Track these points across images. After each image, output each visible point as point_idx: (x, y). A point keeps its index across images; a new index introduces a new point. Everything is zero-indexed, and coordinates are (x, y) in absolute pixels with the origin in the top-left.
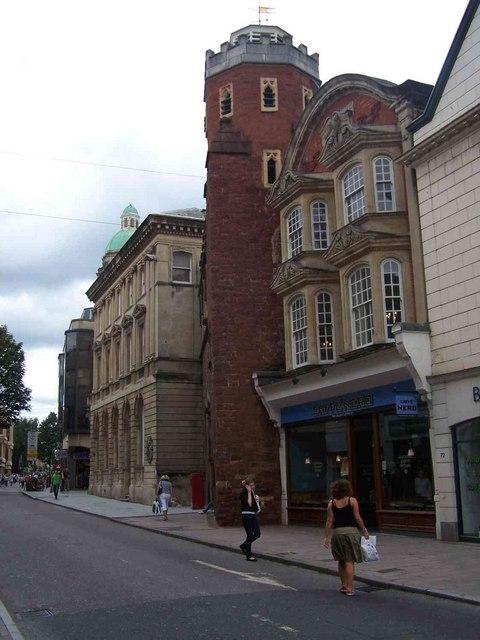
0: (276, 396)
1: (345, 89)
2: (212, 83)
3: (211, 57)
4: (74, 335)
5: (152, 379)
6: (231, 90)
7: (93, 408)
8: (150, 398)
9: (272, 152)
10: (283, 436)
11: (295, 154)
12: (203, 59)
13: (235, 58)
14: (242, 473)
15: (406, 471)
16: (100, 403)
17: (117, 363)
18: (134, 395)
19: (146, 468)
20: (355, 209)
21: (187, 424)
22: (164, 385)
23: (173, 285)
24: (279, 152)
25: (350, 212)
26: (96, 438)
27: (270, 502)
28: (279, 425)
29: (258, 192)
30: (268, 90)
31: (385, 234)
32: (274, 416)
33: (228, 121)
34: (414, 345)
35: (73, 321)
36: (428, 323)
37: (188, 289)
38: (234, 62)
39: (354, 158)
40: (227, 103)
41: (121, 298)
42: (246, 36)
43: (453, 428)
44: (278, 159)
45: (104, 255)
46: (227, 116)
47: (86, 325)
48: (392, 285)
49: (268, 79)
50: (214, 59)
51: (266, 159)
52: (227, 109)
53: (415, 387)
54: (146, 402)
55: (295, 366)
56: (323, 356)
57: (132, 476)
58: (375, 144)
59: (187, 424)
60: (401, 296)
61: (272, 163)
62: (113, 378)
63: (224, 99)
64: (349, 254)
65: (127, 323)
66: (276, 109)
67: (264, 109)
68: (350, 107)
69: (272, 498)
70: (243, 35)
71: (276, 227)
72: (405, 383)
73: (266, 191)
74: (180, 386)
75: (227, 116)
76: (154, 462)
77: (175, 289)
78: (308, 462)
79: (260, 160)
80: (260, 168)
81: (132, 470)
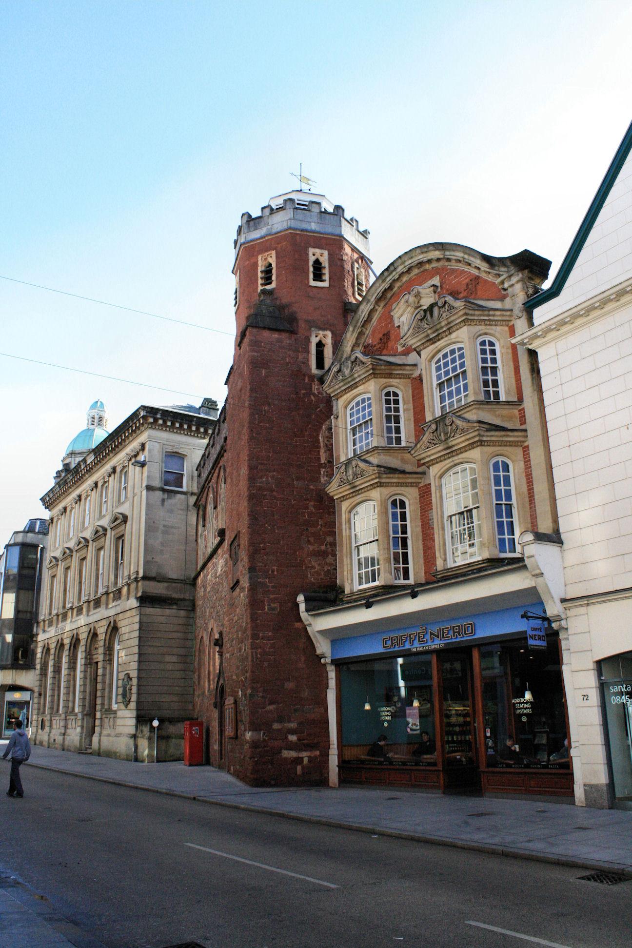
0: (321, 624)
1: (429, 261)
2: (247, 254)
3: (250, 221)
4: (16, 551)
5: (133, 603)
6: (273, 260)
7: (41, 637)
8: (130, 627)
9: (321, 332)
10: (332, 675)
11: (355, 335)
13: (279, 223)
14: (281, 720)
15: (386, 724)
16: (52, 632)
17: (80, 583)
18: (105, 622)
19: (119, 713)
20: (361, 441)
21: (174, 659)
22: (149, 610)
23: (163, 490)
24: (329, 334)
25: (354, 444)
26: (44, 673)
27: (316, 757)
28: (329, 660)
29: (300, 374)
30: (317, 263)
31: (496, 426)
32: (323, 647)
33: (270, 293)
34: (541, 555)
35: (16, 533)
36: (557, 531)
37: (182, 497)
38: (277, 227)
39: (454, 335)
40: (268, 272)
41: (90, 504)
43: (599, 663)
44: (328, 341)
45: (64, 455)
46: (268, 287)
47: (31, 538)
48: (503, 488)
49: (318, 251)
50: (252, 223)
51: (314, 341)
52: (268, 279)
53: (315, 651)
54: (123, 630)
55: (357, 587)
56: (502, 550)
57: (97, 722)
58: (480, 320)
59: (174, 659)
60: (514, 501)
61: (320, 345)
62: (72, 600)
63: (263, 269)
65: (100, 534)
66: (326, 284)
67: (313, 283)
68: (436, 281)
69: (318, 753)
72: (530, 602)
73: (312, 377)
74: (168, 611)
75: (268, 287)
76: (133, 705)
77: (166, 496)
78: (367, 707)
79: (308, 340)
80: (308, 351)
81: (98, 715)
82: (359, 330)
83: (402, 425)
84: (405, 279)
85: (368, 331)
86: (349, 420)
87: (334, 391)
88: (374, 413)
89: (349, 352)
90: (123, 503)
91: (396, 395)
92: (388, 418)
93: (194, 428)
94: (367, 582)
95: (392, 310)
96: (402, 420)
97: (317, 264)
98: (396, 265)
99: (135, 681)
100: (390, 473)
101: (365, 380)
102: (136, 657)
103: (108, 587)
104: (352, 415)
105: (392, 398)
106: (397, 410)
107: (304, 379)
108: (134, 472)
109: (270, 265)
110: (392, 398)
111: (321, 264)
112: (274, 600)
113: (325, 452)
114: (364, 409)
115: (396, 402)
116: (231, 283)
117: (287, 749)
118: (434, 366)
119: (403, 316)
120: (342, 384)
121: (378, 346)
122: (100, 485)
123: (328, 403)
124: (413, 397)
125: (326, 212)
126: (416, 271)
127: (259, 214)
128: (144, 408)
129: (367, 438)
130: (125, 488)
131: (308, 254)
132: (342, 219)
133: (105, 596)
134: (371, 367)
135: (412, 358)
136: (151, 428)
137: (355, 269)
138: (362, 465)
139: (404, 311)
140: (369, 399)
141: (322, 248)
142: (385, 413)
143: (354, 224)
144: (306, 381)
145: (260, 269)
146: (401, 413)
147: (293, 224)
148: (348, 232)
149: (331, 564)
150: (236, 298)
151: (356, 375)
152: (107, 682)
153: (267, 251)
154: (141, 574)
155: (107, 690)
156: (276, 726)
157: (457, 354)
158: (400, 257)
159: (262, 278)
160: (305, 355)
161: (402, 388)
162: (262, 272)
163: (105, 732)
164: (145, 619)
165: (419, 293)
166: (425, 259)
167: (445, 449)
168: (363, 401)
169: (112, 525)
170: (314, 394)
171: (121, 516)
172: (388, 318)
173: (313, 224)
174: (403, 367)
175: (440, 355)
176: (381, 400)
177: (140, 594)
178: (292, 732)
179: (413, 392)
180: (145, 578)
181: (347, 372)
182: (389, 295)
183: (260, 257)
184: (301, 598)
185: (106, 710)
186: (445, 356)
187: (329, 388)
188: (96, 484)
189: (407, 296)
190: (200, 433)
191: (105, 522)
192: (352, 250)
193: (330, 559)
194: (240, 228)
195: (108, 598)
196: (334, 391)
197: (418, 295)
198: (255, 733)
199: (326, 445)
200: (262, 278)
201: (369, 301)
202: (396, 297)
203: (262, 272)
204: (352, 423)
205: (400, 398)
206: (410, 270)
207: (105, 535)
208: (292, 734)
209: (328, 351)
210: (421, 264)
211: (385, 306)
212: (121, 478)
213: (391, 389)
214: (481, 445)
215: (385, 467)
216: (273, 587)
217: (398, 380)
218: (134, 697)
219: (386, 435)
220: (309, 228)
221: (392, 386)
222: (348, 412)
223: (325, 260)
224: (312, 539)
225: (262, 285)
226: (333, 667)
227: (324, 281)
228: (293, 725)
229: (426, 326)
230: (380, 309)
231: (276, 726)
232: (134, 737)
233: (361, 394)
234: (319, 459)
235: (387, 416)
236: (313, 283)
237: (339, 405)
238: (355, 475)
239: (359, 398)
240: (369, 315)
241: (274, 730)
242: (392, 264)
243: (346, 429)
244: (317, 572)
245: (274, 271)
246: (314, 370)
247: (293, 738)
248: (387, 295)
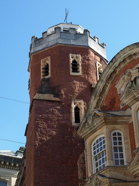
2: (35, 58)
3: (36, 41)
6: (49, 62)
11: (96, 101)
12: (30, 42)
13: (52, 41)
25: (97, 166)
33: (48, 80)
40: (46, 68)
42: (60, 28)
44: (82, 106)
46: (46, 77)
49: (75, 56)
50: (37, 42)
52: (46, 73)
61: (77, 109)
63: (44, 67)
64: (90, 129)
66: (49, 76)
67: (72, 74)
70: (58, 27)
71: (81, 153)
73: (73, 128)
75: (46, 77)
80: (70, 113)
82: (98, 98)
83: (124, 152)
84: (122, 66)
85: (103, 99)
86: (93, 151)
87: (83, 135)
88: (106, 146)
91: (119, 134)
92: (115, 149)
93: (12, 164)
95: (115, 85)
96: (124, 150)
97: (75, 63)
98: (116, 58)
100: (117, 182)
101: (100, 127)
104: (94, 148)
105: (117, 136)
106: (120, 143)
107: (68, 129)
109: (48, 64)
110: (117, 136)
111: (76, 63)
113: (81, 172)
114: (101, 144)
115: (120, 139)
116: (27, 76)
119: (121, 86)
120: (88, 129)
121: (109, 107)
123: (82, 141)
124: (130, 135)
125: (80, 34)
126: (128, 61)
127: (41, 36)
129: (103, 162)
131: (69, 57)
132: (89, 38)
135: (128, 112)
137: (97, 65)
138: (100, 178)
139: (123, 85)
140: (104, 138)
141: (76, 54)
142: (113, 146)
143: (96, 40)
145: (42, 67)
146: (123, 145)
147: (60, 41)
148: (92, 44)
150: (29, 85)
151: (95, 124)
153: (45, 57)
158: (118, 53)
159: (43, 72)
161: (123, 130)
162: (43, 69)
165: (130, 73)
166: (133, 53)
168: (100, 139)
170: (74, 138)
172: (113, 90)
173: (72, 41)
174: (123, 117)
176: (110, 138)
179: (130, 132)
181: (90, 122)
182: (114, 77)
183: (42, 61)
187: (81, 134)
189: (123, 76)
190: (16, 167)
192: (95, 54)
194: (31, 45)
196: (83, 135)
197: (130, 75)
199: (82, 168)
200: (43, 72)
202: (118, 78)
203: (43, 69)
204: (95, 153)
205: (122, 136)
206: (124, 60)
209: (82, 112)
210: (130, 56)
211: (112, 83)
213: (116, 131)
215: (113, 179)
217: (120, 126)
219: (114, 159)
220: (69, 43)
221: (117, 129)
222: (93, 147)
225: (43, 76)
227: (79, 72)
229: (133, 91)
230: (109, 85)
233: (99, 135)
234: (77, 177)
235: (114, 147)
236: (72, 74)
237: (87, 142)
239: (98, 138)
240: (103, 89)
242: (114, 57)
243: (91, 156)
245: (50, 68)
248: (113, 78)
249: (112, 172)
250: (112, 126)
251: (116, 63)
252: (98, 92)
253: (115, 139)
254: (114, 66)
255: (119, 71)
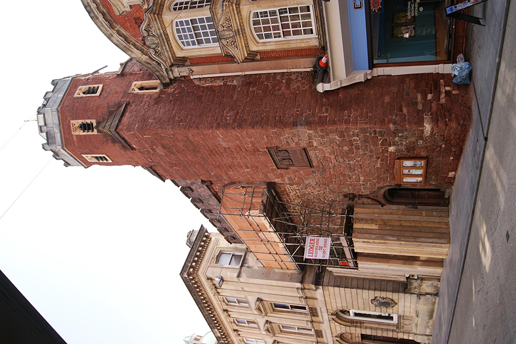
5: (319, 293)
13: (53, 119)
18: (333, 325)
27: (445, 82)
28: (369, 72)
32: (360, 77)
40: (85, 127)
61: (141, 88)
69: (442, 81)
76: (395, 296)
80: (144, 95)
89: (147, 57)
90: (258, 326)
94: (309, 16)
98: (87, 5)
99: (378, 294)
102: (359, 291)
103: (307, 321)
108: (227, 290)
112: (320, 111)
113: (216, 82)
117: (439, 101)
118: (187, 47)
122: (236, 328)
128: (181, 274)
130: (239, 302)
133: (314, 324)
134: (152, 15)
136: (197, 271)
144: (164, 96)
149: (297, 76)
151: (159, 33)
152: (376, 326)
154: (299, 285)
155: (382, 327)
156: (420, 107)
157: (180, 27)
160: (145, 97)
163: (414, 331)
164: (332, 283)
167: (239, 35)
169: (264, 314)
171: (266, 325)
175: (179, 42)
177: (313, 287)
178: (425, 97)
180: (302, 282)
184: (321, 88)
185: (397, 328)
186: (180, 37)
188: (226, 311)
191: (261, 321)
193: (293, 77)
195: (315, 322)
198: (425, 121)
201: (111, 34)
207: (270, 323)
208: (427, 97)
212: (231, 305)
214: (239, 5)
216: (310, 111)
218: (389, 295)
223: (85, 88)
224: (277, 88)
226: (375, 69)
228: (419, 97)
231: (420, 107)
232: (419, 295)
236: (98, 94)
238: (230, 28)
239: (176, 35)
241: (423, 109)
244: (302, 85)
246: (157, 91)
247: (430, 96)
249: (218, 6)
250: (165, 9)
251: (92, 7)
252: (124, 44)
253: (180, 9)
254: (95, 11)
255: (104, 8)
